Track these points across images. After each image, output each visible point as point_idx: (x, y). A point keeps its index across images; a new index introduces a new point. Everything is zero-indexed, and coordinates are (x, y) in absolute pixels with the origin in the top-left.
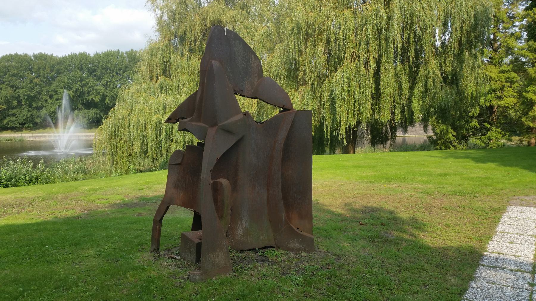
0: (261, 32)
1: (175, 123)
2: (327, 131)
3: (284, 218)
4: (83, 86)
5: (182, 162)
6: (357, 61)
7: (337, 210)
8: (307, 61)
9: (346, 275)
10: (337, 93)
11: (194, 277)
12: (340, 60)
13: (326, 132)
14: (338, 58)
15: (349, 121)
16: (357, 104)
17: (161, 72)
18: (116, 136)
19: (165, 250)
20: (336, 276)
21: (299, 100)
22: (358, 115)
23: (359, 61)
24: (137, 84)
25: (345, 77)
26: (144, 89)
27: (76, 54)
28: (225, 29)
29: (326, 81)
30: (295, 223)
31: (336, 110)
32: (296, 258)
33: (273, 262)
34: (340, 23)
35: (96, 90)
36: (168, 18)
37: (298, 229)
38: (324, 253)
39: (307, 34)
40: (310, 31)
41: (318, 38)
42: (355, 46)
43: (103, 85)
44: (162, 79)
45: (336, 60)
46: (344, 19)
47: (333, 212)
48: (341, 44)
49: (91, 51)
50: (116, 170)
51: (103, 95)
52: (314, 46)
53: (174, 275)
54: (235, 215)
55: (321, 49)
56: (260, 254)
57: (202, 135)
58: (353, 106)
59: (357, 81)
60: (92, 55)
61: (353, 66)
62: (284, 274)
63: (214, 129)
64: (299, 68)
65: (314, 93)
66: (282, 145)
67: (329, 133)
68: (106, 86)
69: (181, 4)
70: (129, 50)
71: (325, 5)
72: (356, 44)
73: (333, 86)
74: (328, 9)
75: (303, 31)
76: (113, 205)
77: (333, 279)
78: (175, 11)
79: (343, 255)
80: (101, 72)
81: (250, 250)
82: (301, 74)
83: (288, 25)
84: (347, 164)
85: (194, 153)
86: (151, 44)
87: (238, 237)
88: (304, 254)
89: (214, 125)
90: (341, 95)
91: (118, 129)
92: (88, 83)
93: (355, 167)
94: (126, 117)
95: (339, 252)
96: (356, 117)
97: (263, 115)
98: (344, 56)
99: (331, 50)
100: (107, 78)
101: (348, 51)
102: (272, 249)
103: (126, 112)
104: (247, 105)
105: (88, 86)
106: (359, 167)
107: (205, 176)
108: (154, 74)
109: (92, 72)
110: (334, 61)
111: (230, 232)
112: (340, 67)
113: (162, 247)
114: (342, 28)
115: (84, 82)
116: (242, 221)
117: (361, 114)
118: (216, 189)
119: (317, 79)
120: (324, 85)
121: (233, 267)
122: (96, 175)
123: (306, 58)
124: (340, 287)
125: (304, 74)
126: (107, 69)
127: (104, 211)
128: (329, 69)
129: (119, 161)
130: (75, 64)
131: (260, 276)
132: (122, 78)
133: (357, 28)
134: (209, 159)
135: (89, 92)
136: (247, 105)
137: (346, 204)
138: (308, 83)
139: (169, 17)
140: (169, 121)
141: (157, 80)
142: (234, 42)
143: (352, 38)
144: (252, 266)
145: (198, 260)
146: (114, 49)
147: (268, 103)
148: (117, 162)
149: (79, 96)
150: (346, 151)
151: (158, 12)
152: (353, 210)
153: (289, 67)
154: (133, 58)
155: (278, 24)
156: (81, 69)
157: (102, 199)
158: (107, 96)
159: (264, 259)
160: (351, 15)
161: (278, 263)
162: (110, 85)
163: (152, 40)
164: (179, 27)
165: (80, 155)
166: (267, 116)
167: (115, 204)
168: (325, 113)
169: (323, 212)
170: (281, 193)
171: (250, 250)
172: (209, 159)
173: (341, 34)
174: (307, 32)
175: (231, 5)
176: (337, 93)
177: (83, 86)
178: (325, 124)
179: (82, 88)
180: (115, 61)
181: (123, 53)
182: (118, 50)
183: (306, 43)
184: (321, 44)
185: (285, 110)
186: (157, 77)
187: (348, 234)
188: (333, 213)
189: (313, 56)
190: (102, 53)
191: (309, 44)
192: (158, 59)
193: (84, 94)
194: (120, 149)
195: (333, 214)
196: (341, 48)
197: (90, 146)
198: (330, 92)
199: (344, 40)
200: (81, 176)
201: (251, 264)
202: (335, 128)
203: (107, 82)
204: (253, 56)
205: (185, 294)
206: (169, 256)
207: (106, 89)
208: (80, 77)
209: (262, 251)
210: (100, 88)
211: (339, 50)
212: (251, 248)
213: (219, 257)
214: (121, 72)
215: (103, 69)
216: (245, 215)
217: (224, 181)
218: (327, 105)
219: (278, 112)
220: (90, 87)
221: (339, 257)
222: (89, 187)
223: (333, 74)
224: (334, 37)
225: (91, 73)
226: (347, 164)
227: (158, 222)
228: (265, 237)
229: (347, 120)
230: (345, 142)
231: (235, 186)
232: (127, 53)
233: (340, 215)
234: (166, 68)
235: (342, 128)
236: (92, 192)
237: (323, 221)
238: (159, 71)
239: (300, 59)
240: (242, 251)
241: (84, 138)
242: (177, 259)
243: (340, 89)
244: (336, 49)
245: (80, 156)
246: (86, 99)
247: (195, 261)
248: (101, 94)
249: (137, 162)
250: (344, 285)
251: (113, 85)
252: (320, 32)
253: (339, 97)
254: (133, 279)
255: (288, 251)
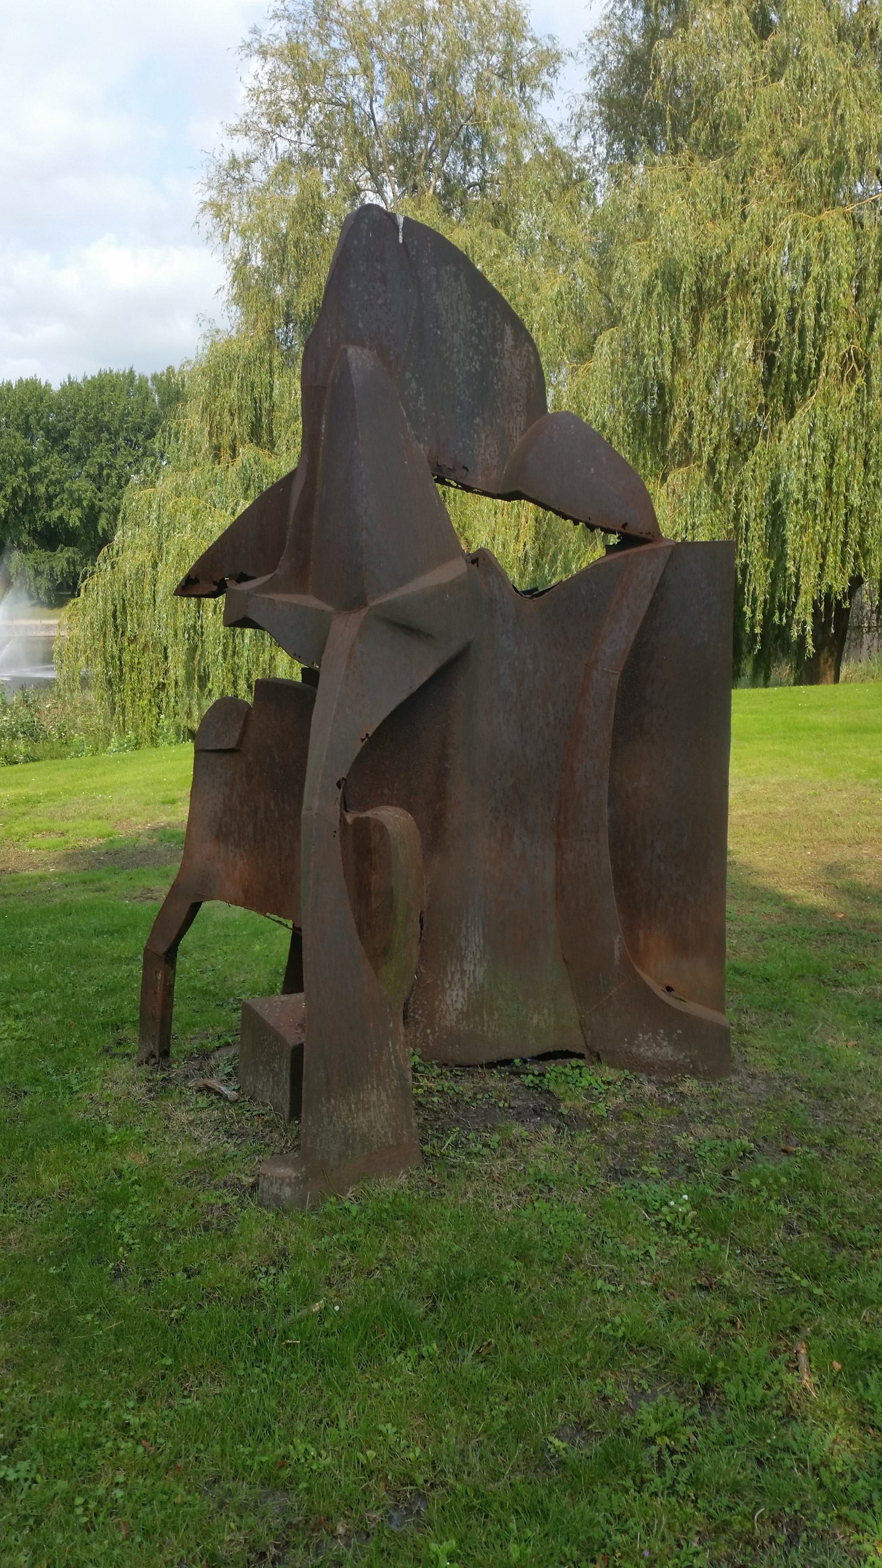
0: (553, 294)
1: (214, 595)
2: (753, 612)
3: (617, 953)
4: (33, 480)
5: (240, 742)
6: (860, 381)
7: (802, 891)
8: (699, 382)
9: (855, 1184)
10: (794, 487)
11: (275, 1190)
12: (806, 378)
13: (749, 614)
14: (800, 371)
15: (827, 580)
16: (854, 524)
17: (246, 429)
18: (119, 630)
19: (190, 1057)
20: (816, 1190)
21: (679, 509)
22: (856, 557)
23: (868, 380)
24: (177, 469)
25: (820, 433)
26: (197, 486)
27: (9, 383)
28: (401, 220)
29: (758, 448)
30: (658, 971)
31: (784, 542)
32: (662, 1103)
33: (572, 1123)
34: (808, 253)
35: (71, 493)
36: (264, 260)
37: (669, 989)
38: (768, 1079)
39: (701, 294)
40: (710, 283)
41: (735, 306)
42: (856, 329)
43: (88, 476)
44: (247, 452)
45: (794, 377)
46: (823, 242)
47: (786, 898)
48: (810, 323)
49: (54, 377)
50: (123, 731)
51: (92, 506)
52: (723, 333)
53: (203, 1171)
54: (436, 938)
55: (743, 345)
56: (528, 1080)
57: (309, 646)
58: (841, 529)
59: (860, 446)
60: (56, 387)
61: (847, 396)
62: (618, 1174)
63: (355, 619)
64: (672, 405)
65: (717, 488)
66: (616, 678)
67: (759, 617)
68: (98, 480)
69: (303, 214)
70: (161, 369)
71: (760, 198)
72: (860, 323)
73: (777, 466)
74: (770, 208)
75: (687, 284)
76: (73, 857)
77: (807, 1199)
78: (286, 236)
79: (837, 1090)
80: (83, 437)
81: (491, 1065)
82: (678, 428)
83: (637, 267)
84: (824, 719)
85: (285, 706)
86: (214, 342)
87: (449, 1021)
88: (690, 1085)
89: (354, 603)
90: (806, 494)
91: (124, 607)
92: (46, 470)
93: (852, 730)
94: (144, 574)
95: (822, 1078)
96: (850, 566)
97: (553, 561)
98: (818, 363)
99: (777, 343)
100: (100, 455)
101: (830, 348)
102: (574, 1062)
103: (144, 557)
104: (496, 528)
105: (46, 481)
106: (866, 730)
107: (316, 803)
108: (226, 440)
109: (57, 438)
110: (785, 382)
111: (415, 1008)
112: (804, 400)
113: (184, 1042)
114: (815, 269)
115: (35, 469)
116: (461, 960)
117: (866, 553)
118: (363, 848)
119: (727, 443)
120: (750, 463)
121: (424, 1142)
122: (61, 748)
123: (696, 373)
124: (837, 1243)
125: (689, 427)
126: (99, 427)
127: (42, 879)
128: (767, 408)
129: (128, 704)
130: (7, 416)
131: (522, 1186)
132: (144, 454)
133: (862, 274)
134: (334, 736)
135: (50, 499)
136: (496, 528)
137: (831, 870)
138: (700, 457)
139: (268, 257)
140: (189, 587)
141: (233, 457)
142: (433, 271)
143: (847, 302)
144: (497, 1137)
145: (295, 1112)
146: (119, 367)
147: (565, 517)
148: (124, 708)
149: (24, 510)
150: (809, 674)
151: (236, 242)
152: (856, 893)
153: (638, 405)
154: (172, 392)
155: (605, 266)
156: (27, 431)
157: (50, 831)
158: (101, 509)
159: (544, 1107)
160: (844, 227)
161: (594, 1124)
162: (109, 476)
163: (217, 331)
164: (298, 286)
165: (22, 685)
166: (566, 569)
167: (83, 852)
168: (748, 553)
169: (753, 900)
170: (607, 862)
171: (491, 1065)
172: (334, 736)
173: (811, 289)
174: (699, 289)
175: (457, 211)
176: (794, 487)
177: (33, 480)
178: (748, 588)
179: (31, 485)
180: (122, 403)
181: (143, 379)
182: (131, 372)
183: (696, 324)
184: (744, 325)
185: (628, 541)
186: (234, 449)
187: (850, 997)
188: (790, 908)
189: (717, 365)
190: (85, 378)
191: (706, 327)
192: (233, 393)
193: (36, 504)
194: (132, 668)
195: (789, 909)
196: (809, 337)
197: (48, 659)
198: (767, 485)
199: (818, 309)
200: (22, 748)
201: (493, 1130)
202: (780, 603)
203: (101, 467)
204: (508, 330)
205: (233, 1270)
206: (201, 1082)
207: (99, 489)
208: (24, 453)
209: (536, 1068)
210: (83, 486)
211: (802, 344)
212: (494, 1056)
213: (374, 1112)
214: (141, 437)
215: (88, 429)
216: (474, 941)
217: (392, 818)
218: (758, 529)
219: (600, 552)
220: (52, 483)
221: (823, 1096)
222: (17, 791)
223: (782, 424)
224: (787, 303)
225: (55, 441)
226: (824, 719)
227: (164, 956)
228: (547, 1018)
229: (820, 577)
230: (810, 647)
231: (435, 833)
232: (155, 377)
233: (813, 912)
234: (259, 419)
235: (802, 600)
236: (22, 809)
237: (752, 938)
238: (240, 427)
239: (677, 377)
240: (466, 1067)
241: (43, 633)
242: (226, 1099)
243: (801, 475)
244: (792, 341)
245: (23, 688)
246: (42, 518)
247: (287, 1113)
248: (85, 503)
249: (181, 709)
250: (853, 1232)
251: (119, 478)
252: (743, 287)
253: (797, 502)
254: (56, 1181)
255: (631, 1071)
